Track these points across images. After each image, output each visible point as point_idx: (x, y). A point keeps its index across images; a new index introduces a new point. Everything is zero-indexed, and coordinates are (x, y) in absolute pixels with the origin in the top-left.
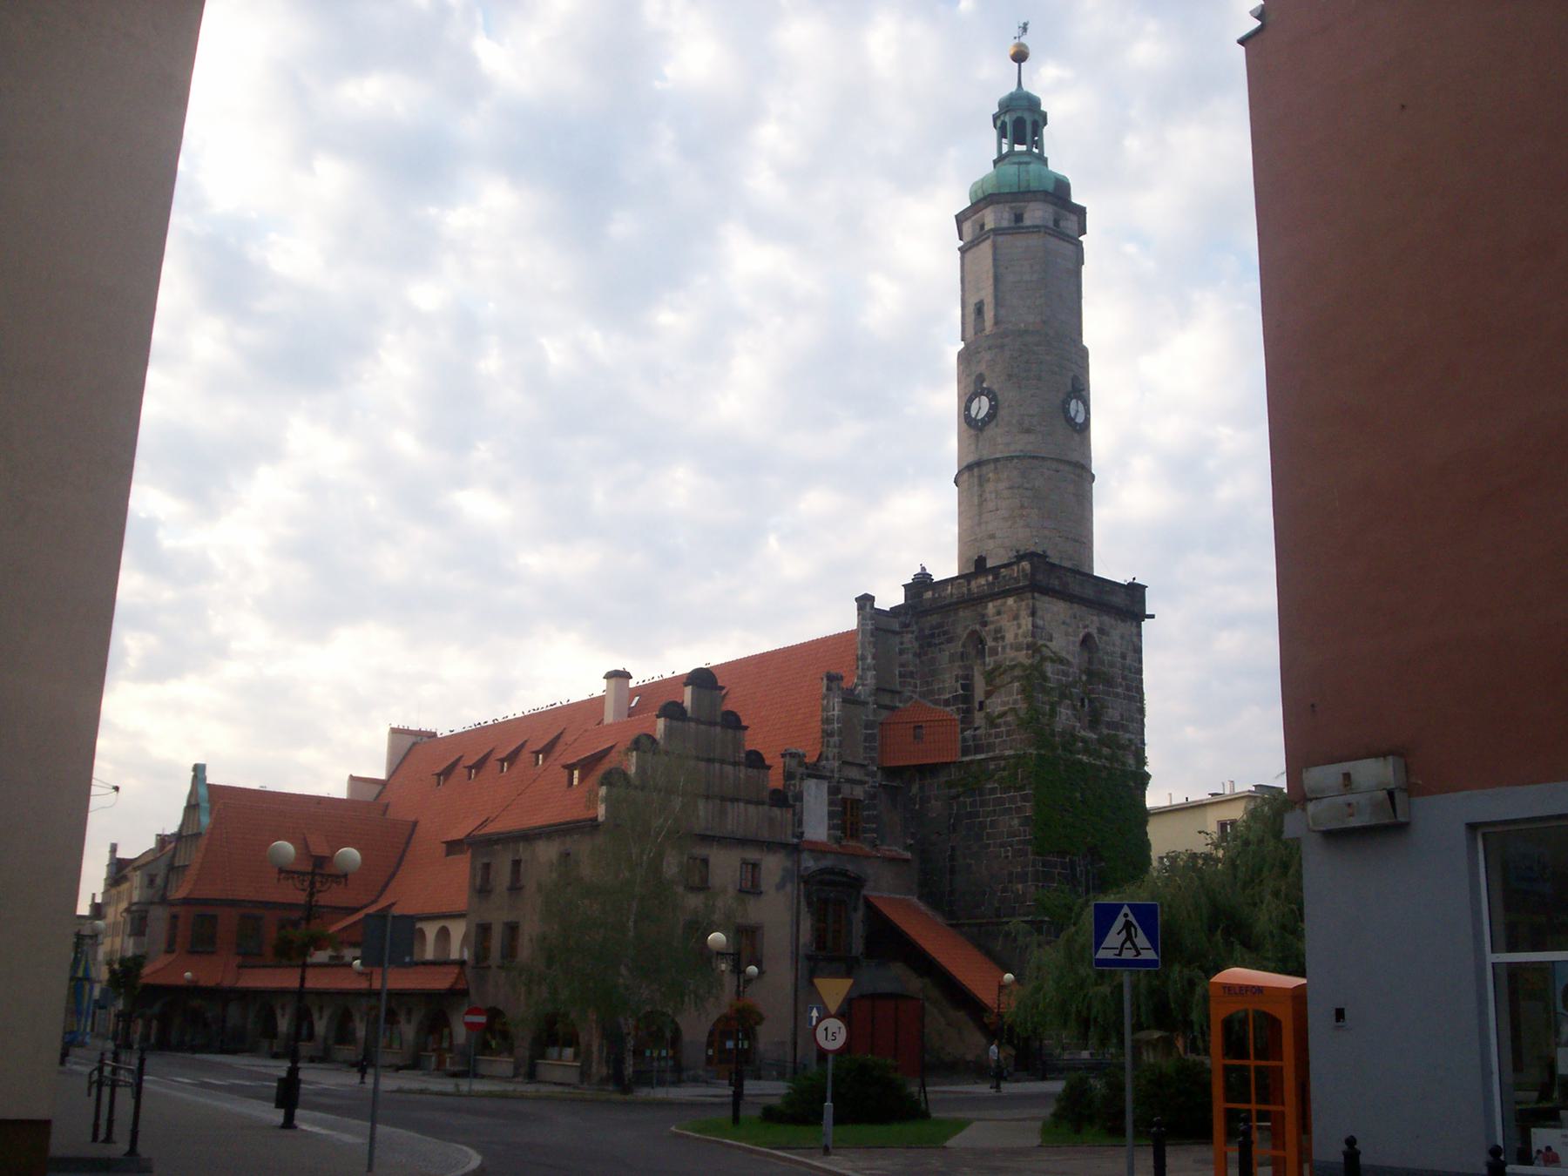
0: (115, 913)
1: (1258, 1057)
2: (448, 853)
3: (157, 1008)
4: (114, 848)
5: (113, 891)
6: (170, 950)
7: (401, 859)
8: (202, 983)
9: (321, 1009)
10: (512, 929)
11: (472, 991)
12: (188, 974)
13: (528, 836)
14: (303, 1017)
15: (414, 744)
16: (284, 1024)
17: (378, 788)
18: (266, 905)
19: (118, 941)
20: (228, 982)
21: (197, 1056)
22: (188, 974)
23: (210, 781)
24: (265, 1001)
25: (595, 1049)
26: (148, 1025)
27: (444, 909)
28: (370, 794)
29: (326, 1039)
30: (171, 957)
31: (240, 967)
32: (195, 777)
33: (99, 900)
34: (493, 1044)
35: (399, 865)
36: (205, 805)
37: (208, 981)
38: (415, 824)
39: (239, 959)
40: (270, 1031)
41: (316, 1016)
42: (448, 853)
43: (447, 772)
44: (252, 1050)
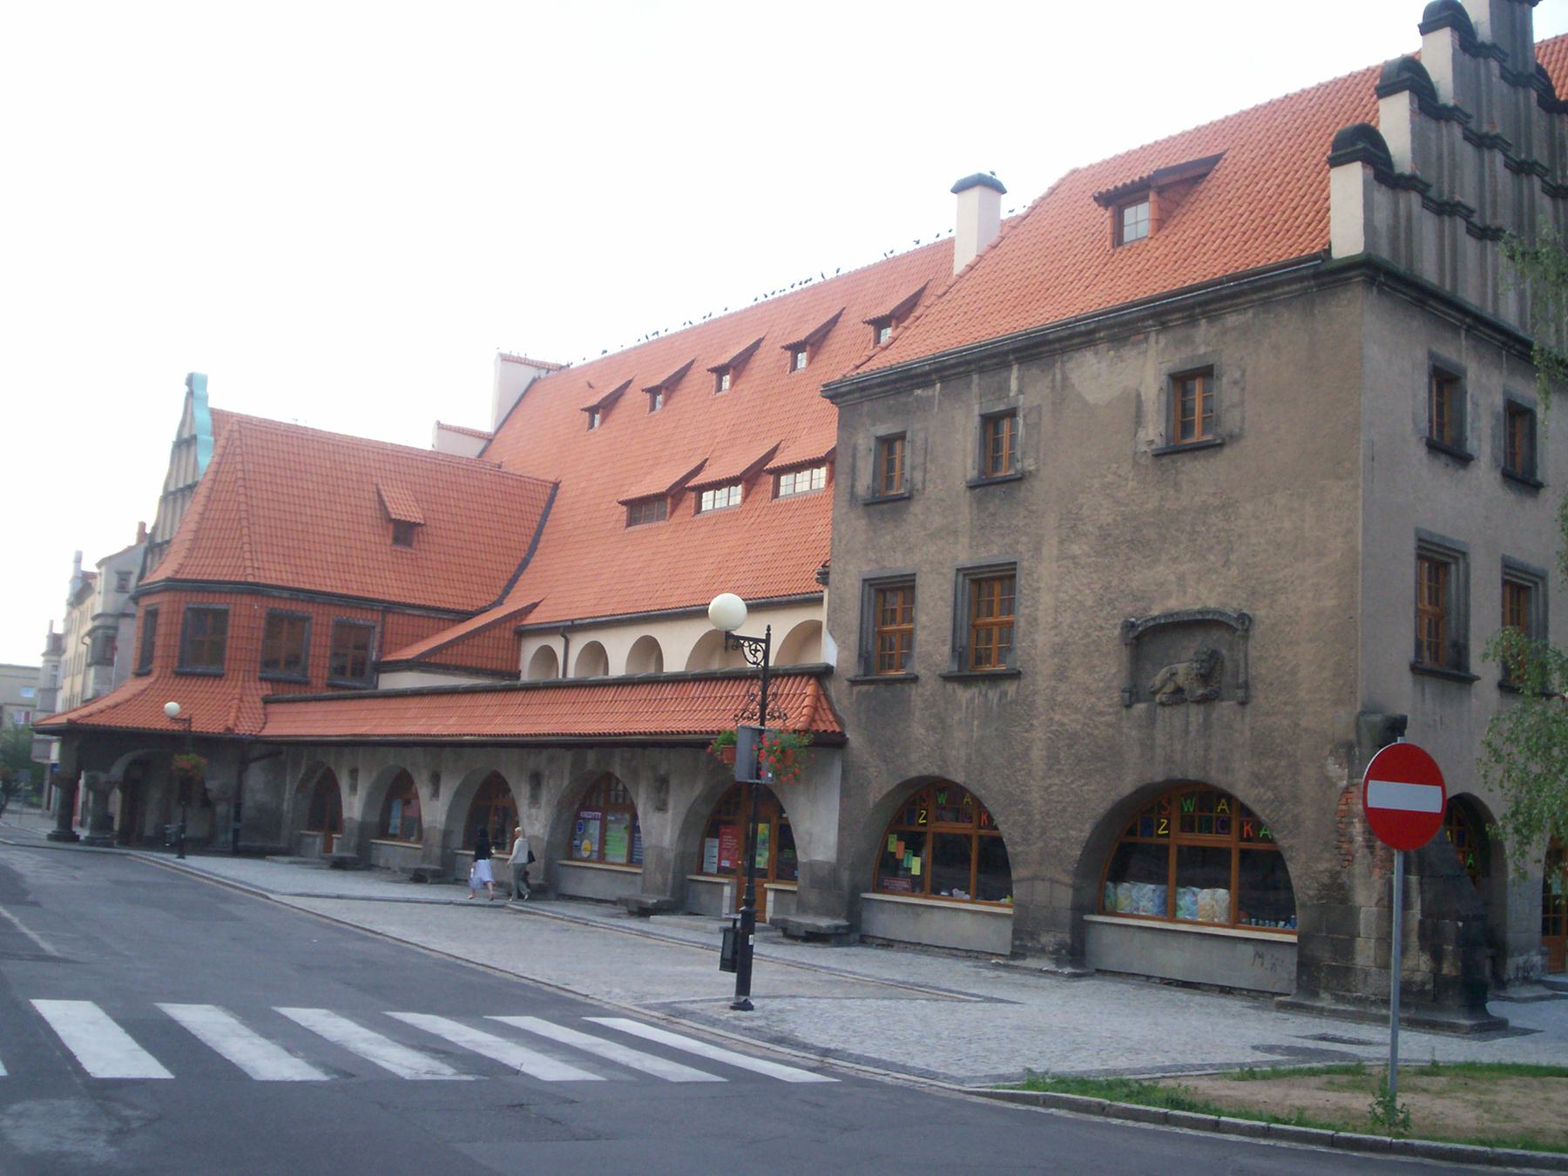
0: (77, 648)
1: (1226, 853)
2: (631, 522)
3: (117, 770)
4: (78, 560)
5: (76, 613)
6: (142, 673)
7: (536, 541)
8: (197, 727)
9: (436, 780)
10: (989, 587)
11: (854, 738)
12: (172, 707)
13: (1039, 349)
14: (398, 789)
15: (534, 381)
16: (354, 806)
17: (481, 444)
18: (312, 596)
19: (79, 680)
20: (246, 728)
21: (195, 862)
22: (172, 707)
23: (214, 403)
24: (317, 764)
25: (1365, 899)
26: (102, 796)
27: (645, 606)
28: (472, 449)
29: (447, 834)
30: (143, 683)
31: (267, 701)
32: (191, 394)
33: (59, 629)
34: (915, 865)
35: (532, 550)
36: (205, 438)
37: (208, 722)
38: (556, 486)
39: (266, 690)
40: (325, 815)
41: (424, 791)
42: (631, 522)
43: (606, 406)
44: (288, 850)
